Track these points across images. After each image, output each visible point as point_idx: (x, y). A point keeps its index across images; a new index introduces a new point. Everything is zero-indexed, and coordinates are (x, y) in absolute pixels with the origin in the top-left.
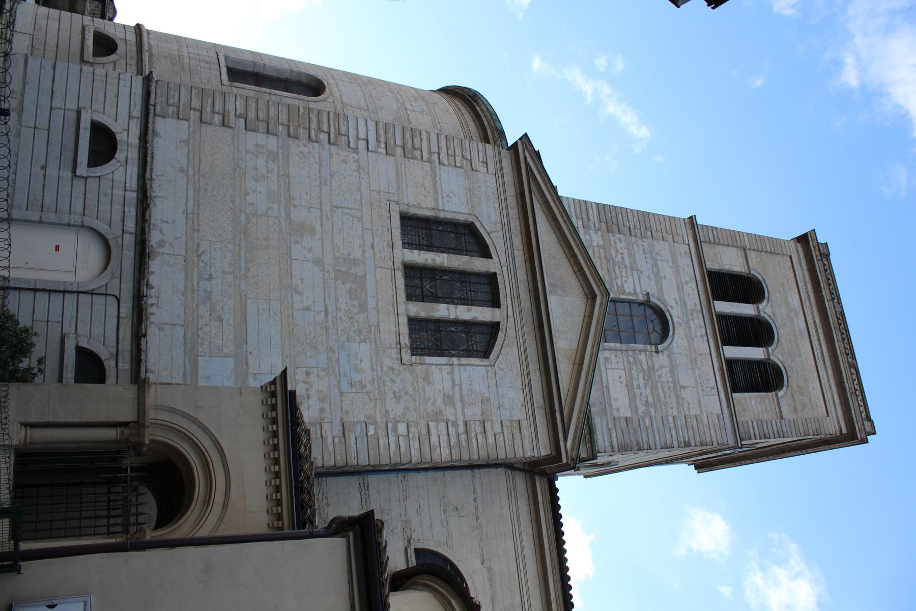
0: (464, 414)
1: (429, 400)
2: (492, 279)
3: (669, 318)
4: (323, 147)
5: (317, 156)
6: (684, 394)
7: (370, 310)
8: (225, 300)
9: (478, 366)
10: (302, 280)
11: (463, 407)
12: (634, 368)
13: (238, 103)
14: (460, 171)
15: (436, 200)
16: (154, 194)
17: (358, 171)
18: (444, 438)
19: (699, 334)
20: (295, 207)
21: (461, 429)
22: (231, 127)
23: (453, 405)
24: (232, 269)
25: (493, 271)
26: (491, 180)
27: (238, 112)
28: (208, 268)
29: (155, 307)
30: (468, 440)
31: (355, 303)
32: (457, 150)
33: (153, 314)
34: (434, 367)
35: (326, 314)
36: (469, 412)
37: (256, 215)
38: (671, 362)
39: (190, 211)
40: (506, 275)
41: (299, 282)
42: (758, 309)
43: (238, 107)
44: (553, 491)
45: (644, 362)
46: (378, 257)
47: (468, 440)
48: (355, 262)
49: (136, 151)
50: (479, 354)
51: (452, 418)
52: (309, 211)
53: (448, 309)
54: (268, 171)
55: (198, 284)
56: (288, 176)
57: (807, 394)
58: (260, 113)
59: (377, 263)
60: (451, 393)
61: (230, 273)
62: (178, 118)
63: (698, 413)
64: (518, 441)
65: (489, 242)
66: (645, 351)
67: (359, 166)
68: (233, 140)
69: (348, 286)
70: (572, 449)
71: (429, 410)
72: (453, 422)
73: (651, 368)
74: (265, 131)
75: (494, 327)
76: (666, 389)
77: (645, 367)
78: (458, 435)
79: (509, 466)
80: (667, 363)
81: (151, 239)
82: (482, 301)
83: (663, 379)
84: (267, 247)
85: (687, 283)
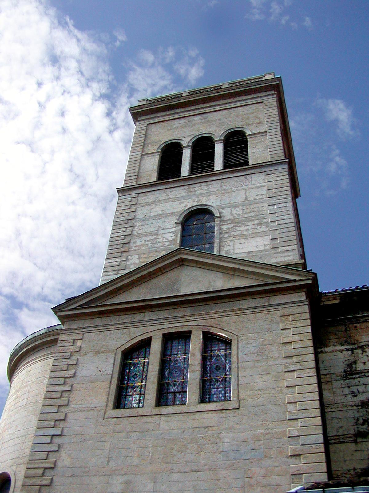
45: (228, 226)
75: (210, 339)
76: (248, 211)
77: (232, 225)
83: (240, 212)
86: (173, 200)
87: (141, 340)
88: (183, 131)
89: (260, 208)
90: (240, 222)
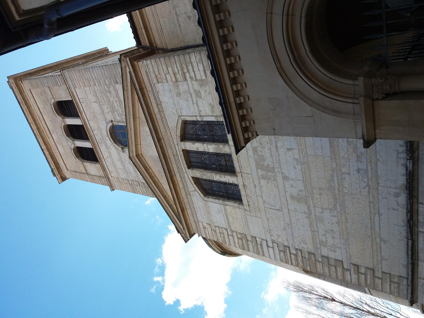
0: (188, 85)
1: (209, 94)
2: (190, 165)
3: (111, 139)
4: (293, 246)
5: (295, 241)
6: (94, 99)
7: (251, 149)
8: (347, 156)
9: (186, 116)
10: (295, 168)
11: (189, 90)
12: (120, 112)
13: (349, 278)
14: (217, 225)
15: (225, 210)
16: (405, 228)
17: (270, 230)
18: (196, 69)
19: (96, 131)
20: (305, 212)
21: (187, 75)
22: (353, 264)
23: (195, 91)
24: (343, 176)
25: (190, 170)
26: (200, 219)
27: (349, 272)
28: (361, 177)
29: (400, 151)
30: (182, 69)
31: (260, 153)
32: (219, 236)
33: (401, 146)
34: (210, 115)
35: (276, 146)
36: (186, 86)
37: (330, 210)
38: (105, 116)
39: (377, 215)
40: (183, 168)
41: (296, 166)
42: (74, 144)
43: (349, 276)
44: (137, 37)
45: (117, 116)
46: (251, 180)
47: (182, 69)
48: (264, 177)
49: (420, 258)
50: (189, 122)
51: (194, 82)
52: (296, 209)
53: (208, 149)
54: (325, 235)
55: (367, 167)
56: (312, 231)
57: (44, 101)
58: (334, 270)
59: (251, 177)
60: (197, 98)
61: (344, 173)
62: (390, 274)
63: (85, 88)
64: (156, 70)
65: (195, 186)
66: (118, 122)
67: (270, 232)
68: (350, 256)
69: (266, 164)
70: (125, 67)
71: (207, 87)
72: (193, 80)
73: (113, 112)
74: (329, 259)
76: (103, 101)
77: (116, 113)
78: (188, 71)
79: (165, 51)
80: (107, 115)
81: (405, 198)
82: (192, 153)
83: (106, 106)
84: (320, 189)
85: (108, 157)
86: (110, 153)
87: (195, 183)
88: (65, 146)
89: (99, 91)
90: (112, 107)
